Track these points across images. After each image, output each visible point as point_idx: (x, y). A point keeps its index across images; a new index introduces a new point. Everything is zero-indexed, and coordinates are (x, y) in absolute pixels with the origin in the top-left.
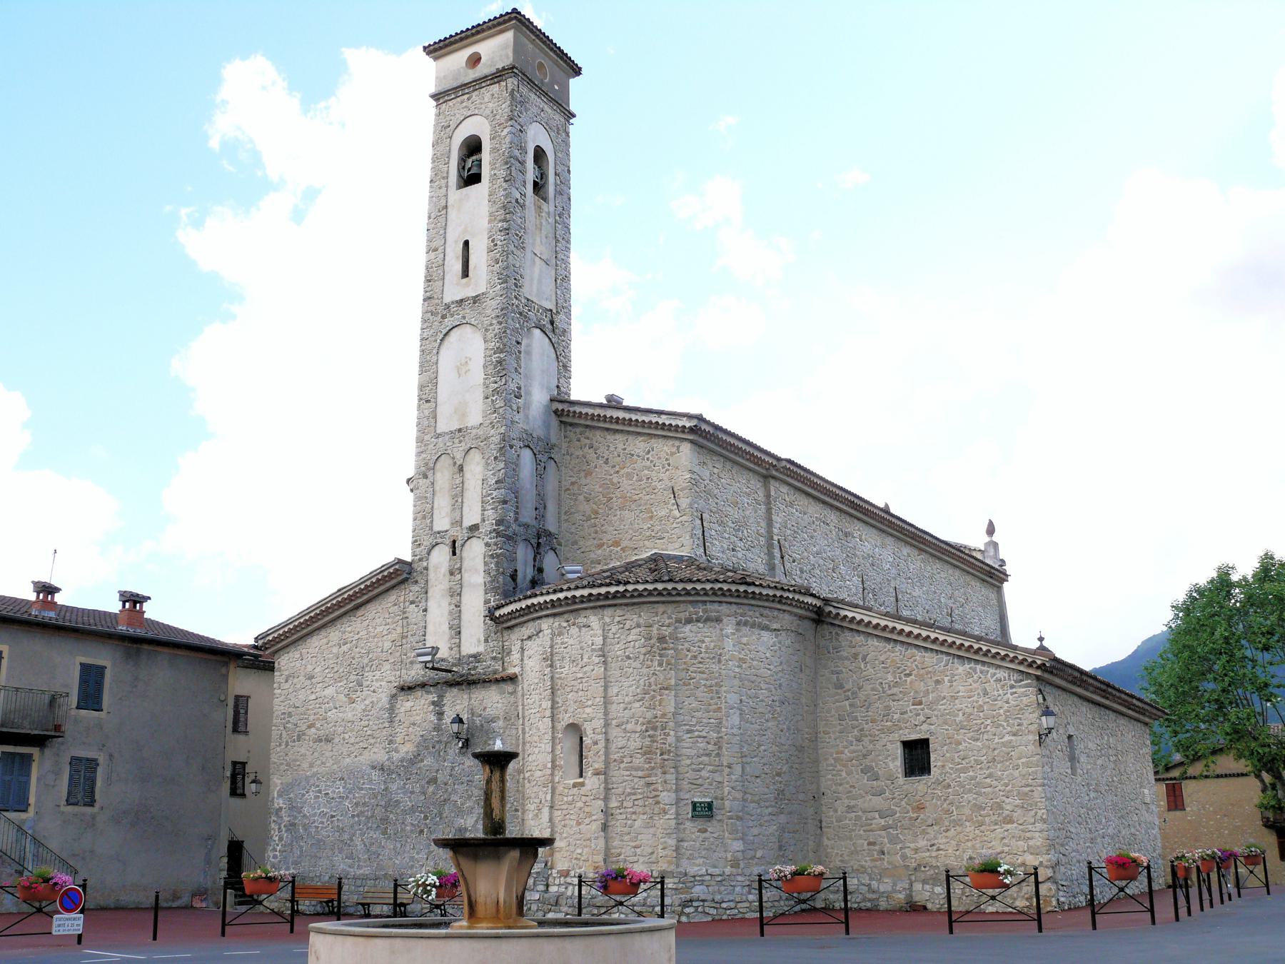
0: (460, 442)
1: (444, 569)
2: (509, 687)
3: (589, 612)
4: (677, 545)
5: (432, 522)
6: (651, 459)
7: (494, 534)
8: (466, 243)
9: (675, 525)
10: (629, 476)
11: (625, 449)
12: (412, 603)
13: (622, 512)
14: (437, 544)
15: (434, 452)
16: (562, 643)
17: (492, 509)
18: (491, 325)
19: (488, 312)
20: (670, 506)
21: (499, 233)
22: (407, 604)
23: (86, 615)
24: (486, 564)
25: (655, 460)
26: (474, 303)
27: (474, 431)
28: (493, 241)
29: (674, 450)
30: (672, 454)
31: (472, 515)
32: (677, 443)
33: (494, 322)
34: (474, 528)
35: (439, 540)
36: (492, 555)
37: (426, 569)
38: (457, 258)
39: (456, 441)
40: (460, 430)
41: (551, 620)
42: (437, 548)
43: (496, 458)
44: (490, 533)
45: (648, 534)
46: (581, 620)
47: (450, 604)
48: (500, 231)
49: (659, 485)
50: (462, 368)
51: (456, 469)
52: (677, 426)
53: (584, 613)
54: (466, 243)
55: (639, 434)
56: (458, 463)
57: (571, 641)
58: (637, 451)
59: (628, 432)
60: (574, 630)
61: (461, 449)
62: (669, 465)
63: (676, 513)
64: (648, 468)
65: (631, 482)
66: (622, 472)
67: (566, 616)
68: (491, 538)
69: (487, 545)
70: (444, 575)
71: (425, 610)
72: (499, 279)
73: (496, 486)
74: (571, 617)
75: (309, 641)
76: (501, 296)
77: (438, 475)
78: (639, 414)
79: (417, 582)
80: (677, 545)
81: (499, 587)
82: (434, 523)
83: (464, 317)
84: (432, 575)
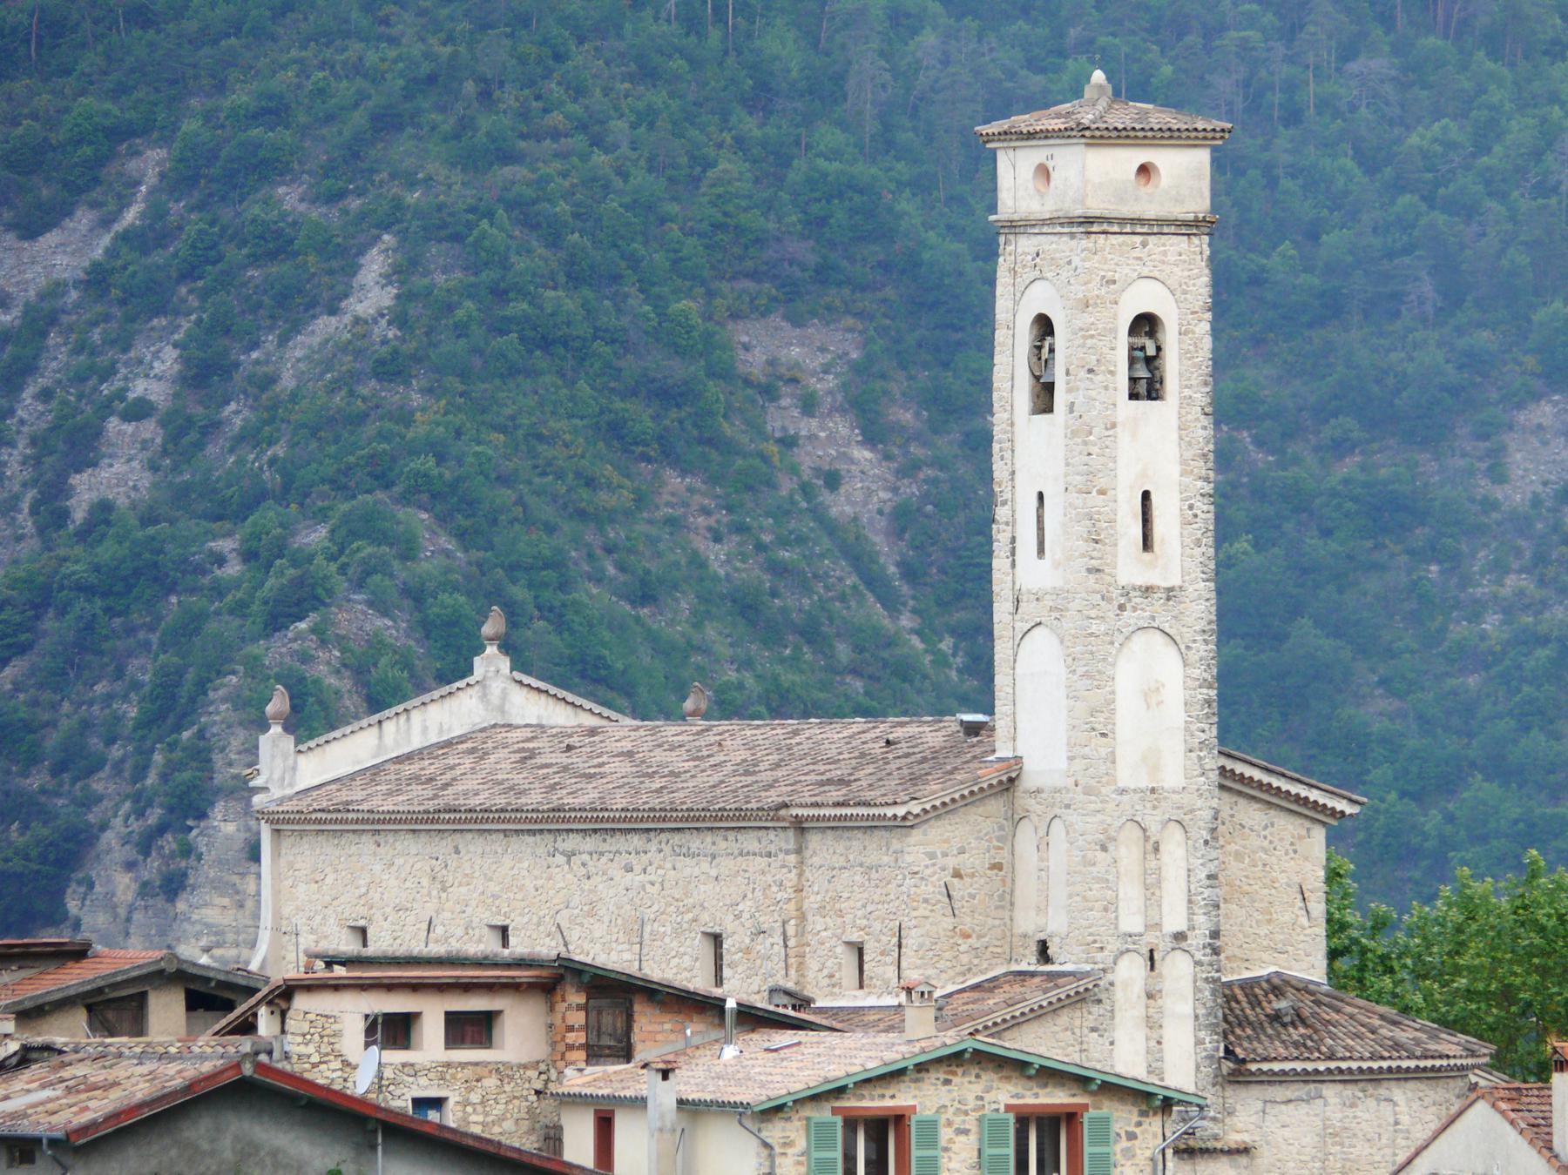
0: (1155, 808)
1: (1138, 988)
2: (1243, 1160)
3: (1393, 1083)
4: (1305, 965)
5: (1117, 918)
6: (1269, 838)
7: (1208, 951)
8: (1146, 496)
9: (1302, 938)
10: (1238, 856)
11: (1232, 816)
12: (1093, 1030)
13: (1229, 906)
14: (1128, 951)
15: (1116, 814)
16: (1355, 1117)
17: (1205, 914)
18: (1195, 641)
19: (1190, 620)
20: (1296, 910)
21: (1199, 497)
22: (1086, 1031)
23: (1547, 1130)
24: (1197, 990)
25: (1276, 843)
26: (1168, 599)
27: (1175, 797)
28: (1191, 507)
29: (1304, 832)
30: (1301, 838)
31: (1175, 920)
32: (1308, 824)
33: (1199, 638)
34: (1180, 937)
35: (1132, 947)
36: (1207, 979)
37: (1112, 984)
38: (1163, 540)
39: (1149, 805)
40: (1153, 790)
41: (1340, 1087)
42: (1126, 957)
43: (1206, 842)
44: (1204, 947)
45: (1265, 943)
46: (1382, 1091)
47: (1147, 1039)
48: (1202, 495)
49: (1283, 879)
50: (1151, 695)
51: (1149, 847)
52: (1333, 809)
53: (1385, 1084)
54: (1146, 496)
55: (1253, 798)
56: (1153, 839)
57: (1366, 1116)
58: (1251, 823)
59: (1240, 793)
60: (1371, 1103)
61: (1158, 818)
62: (1295, 852)
63: (1304, 921)
64: (1266, 851)
65: (1242, 866)
66: (1229, 848)
67: (1361, 1085)
68: (1204, 955)
69: (1198, 963)
70: (1139, 997)
71: (1112, 1043)
72: (1203, 573)
73: (1209, 882)
74: (1370, 1088)
75: (70, 964)
76: (1207, 600)
77: (1123, 851)
78: (1283, 779)
79: (1099, 1001)
80: (1305, 965)
81: (1217, 1025)
82: (1120, 918)
83: (1153, 618)
84: (1119, 994)
